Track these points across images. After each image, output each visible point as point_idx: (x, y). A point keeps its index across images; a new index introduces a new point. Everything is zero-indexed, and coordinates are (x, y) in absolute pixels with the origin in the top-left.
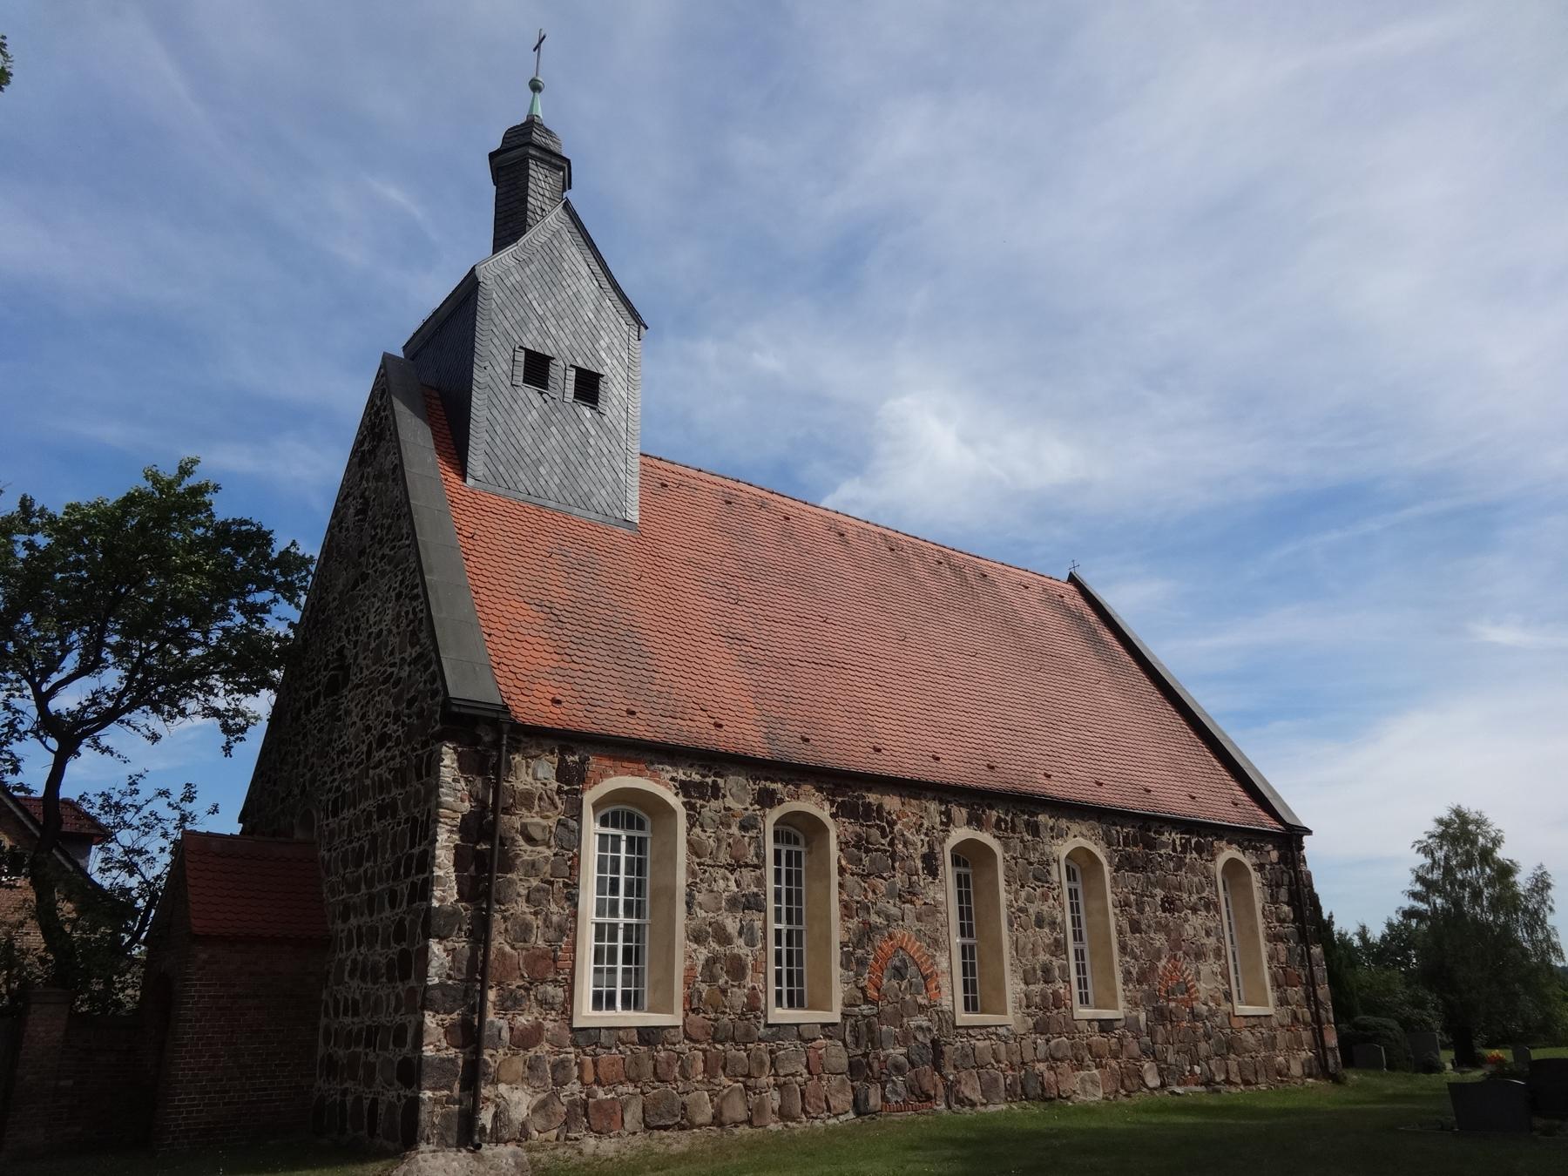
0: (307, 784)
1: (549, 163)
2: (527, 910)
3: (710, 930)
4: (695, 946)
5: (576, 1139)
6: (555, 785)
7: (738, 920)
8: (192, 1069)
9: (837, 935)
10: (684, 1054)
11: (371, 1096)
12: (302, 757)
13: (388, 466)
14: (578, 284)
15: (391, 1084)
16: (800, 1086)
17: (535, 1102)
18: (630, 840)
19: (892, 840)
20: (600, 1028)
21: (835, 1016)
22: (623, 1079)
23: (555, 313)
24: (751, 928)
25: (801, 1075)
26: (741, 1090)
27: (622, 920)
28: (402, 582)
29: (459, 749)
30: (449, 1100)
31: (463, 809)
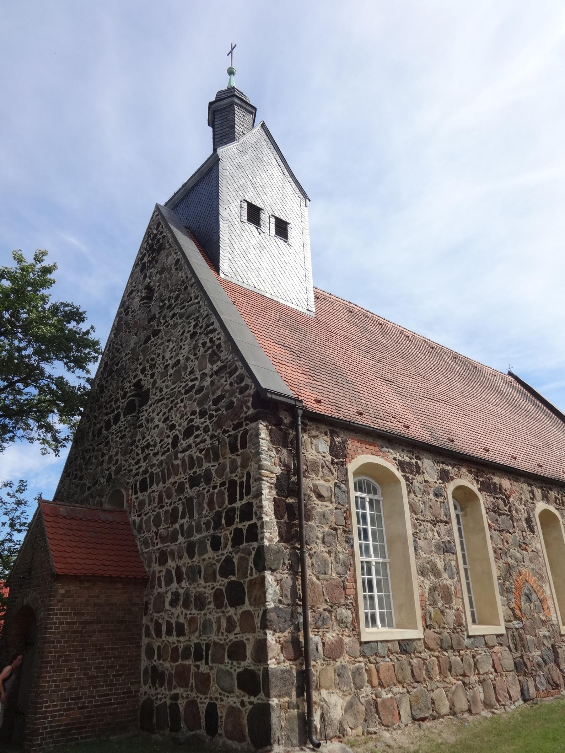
0: (113, 474)
1: (245, 109)
2: (324, 549)
3: (429, 566)
4: (422, 578)
5: (375, 733)
6: (329, 458)
7: (442, 560)
8: (55, 681)
9: (495, 573)
10: (426, 660)
11: (207, 701)
12: (107, 458)
13: (171, 260)
14: (272, 170)
15: (231, 691)
16: (492, 681)
17: (345, 704)
18: (371, 501)
19: (510, 507)
20: (377, 642)
21: (502, 630)
22: (395, 681)
23: (261, 184)
24: (450, 566)
25: (491, 673)
26: (461, 686)
27: (373, 559)
28: (195, 327)
29: (270, 427)
30: (290, 706)
31: (277, 472)
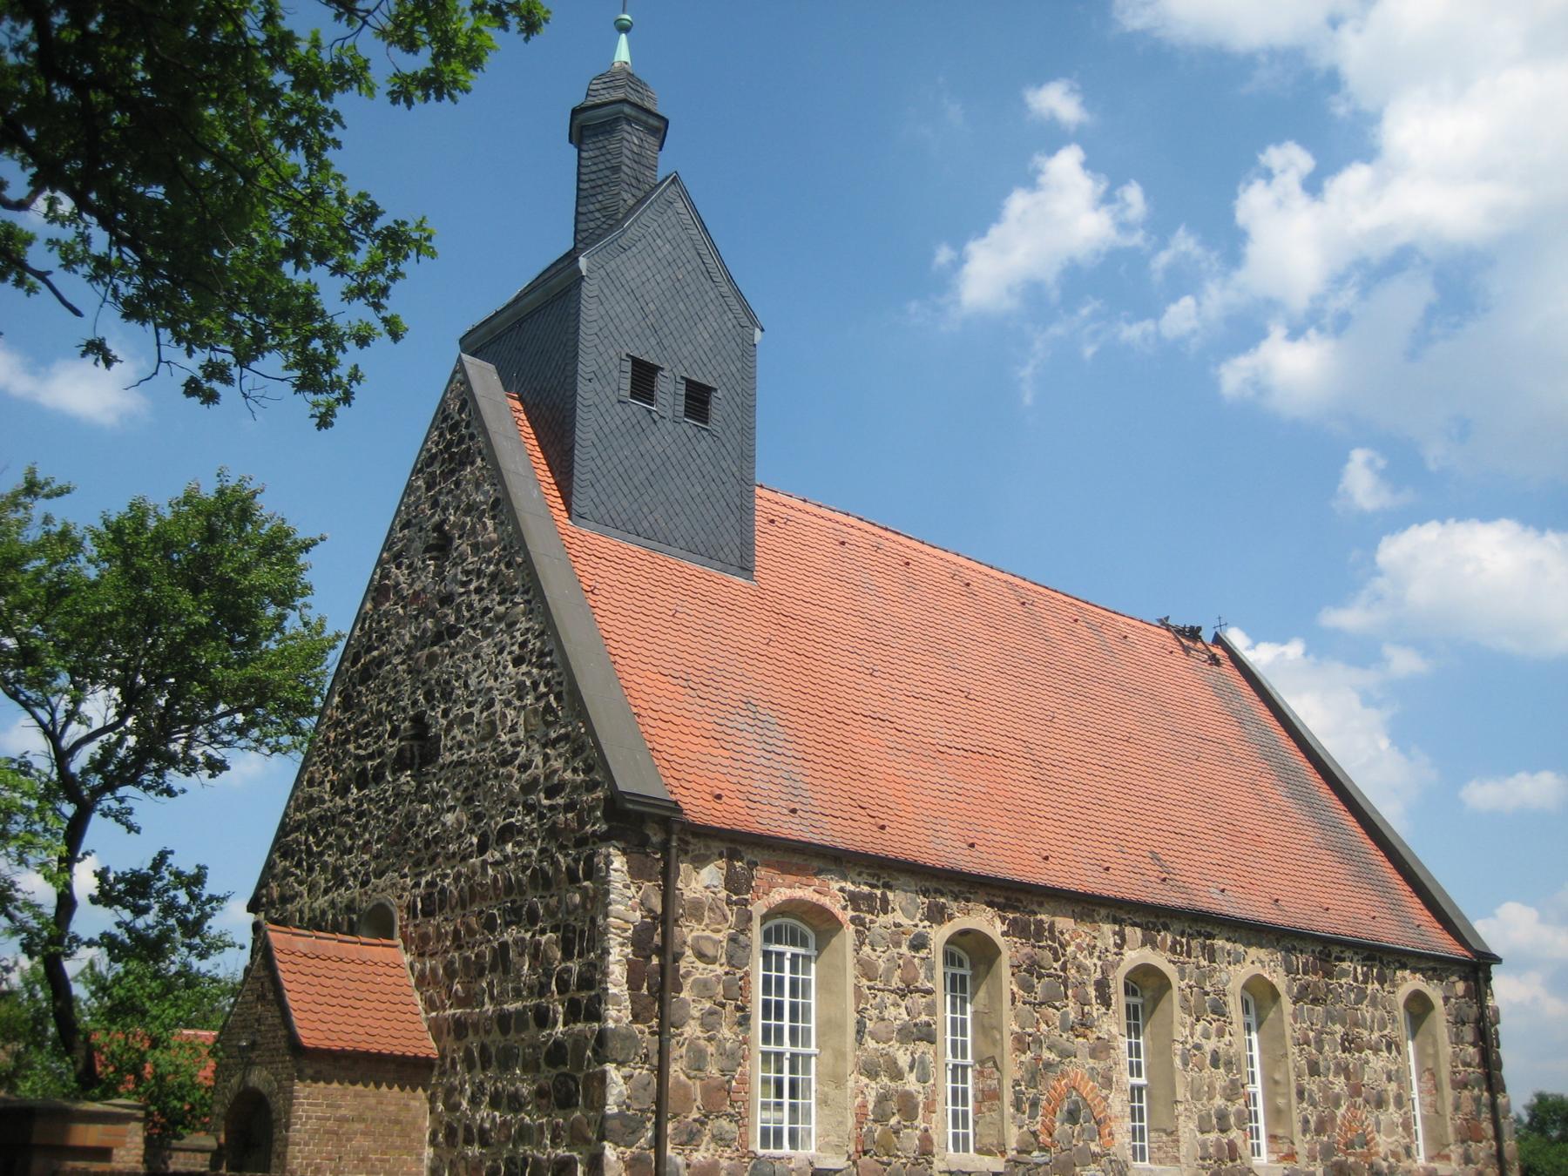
6: (723, 894)
